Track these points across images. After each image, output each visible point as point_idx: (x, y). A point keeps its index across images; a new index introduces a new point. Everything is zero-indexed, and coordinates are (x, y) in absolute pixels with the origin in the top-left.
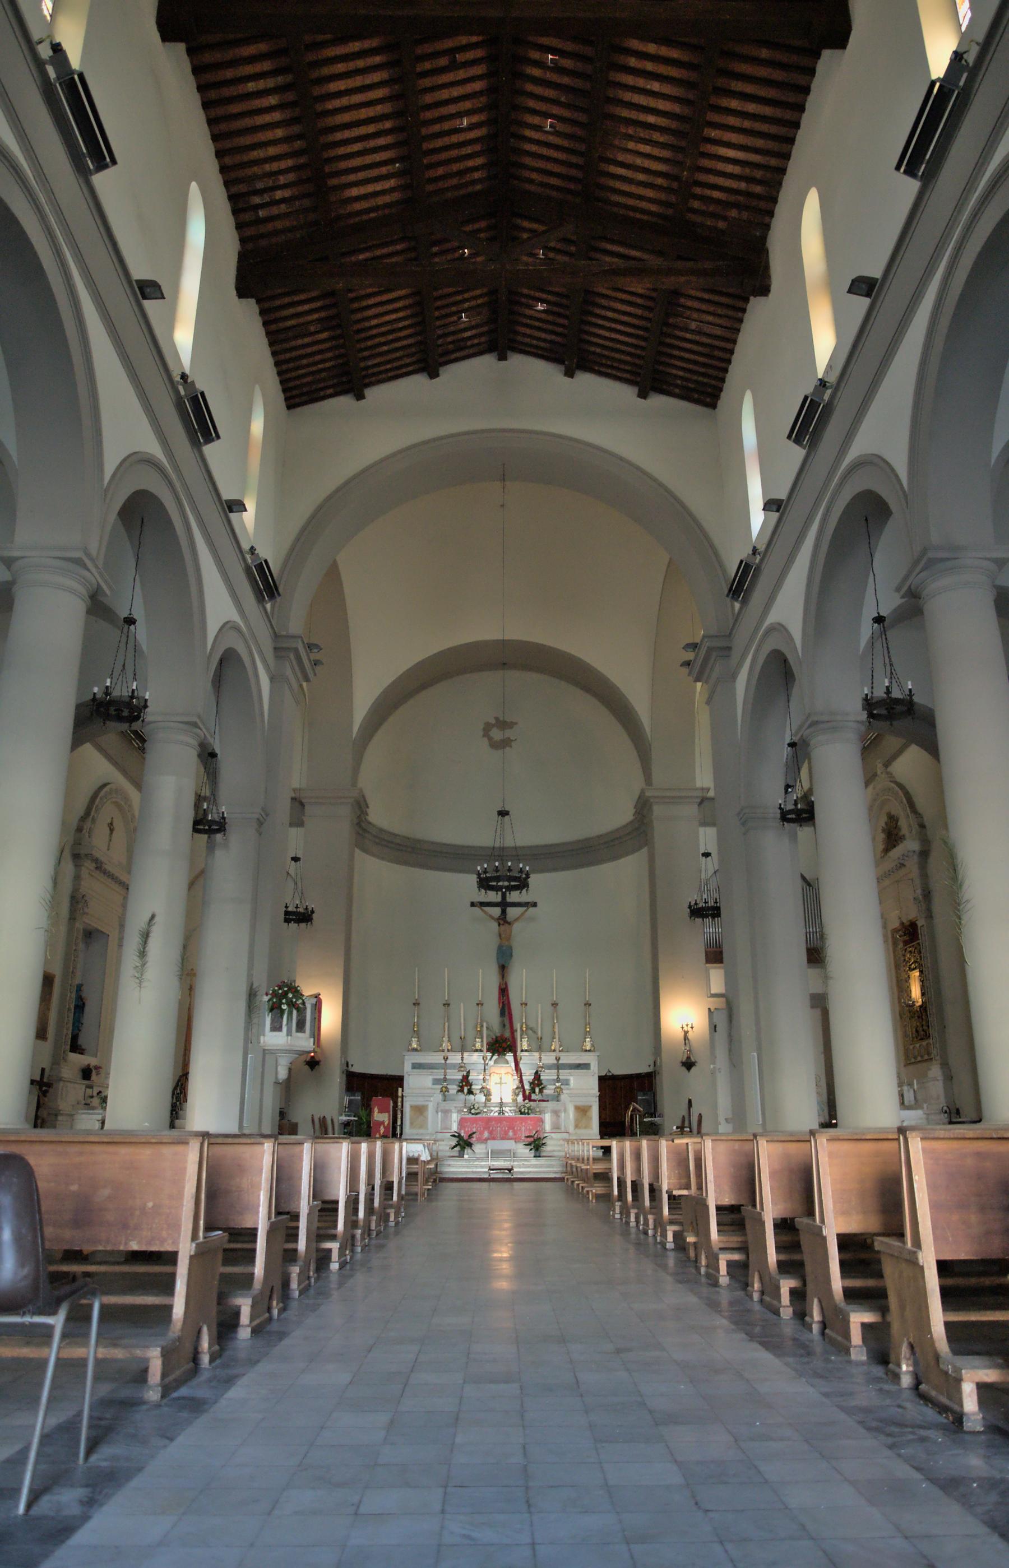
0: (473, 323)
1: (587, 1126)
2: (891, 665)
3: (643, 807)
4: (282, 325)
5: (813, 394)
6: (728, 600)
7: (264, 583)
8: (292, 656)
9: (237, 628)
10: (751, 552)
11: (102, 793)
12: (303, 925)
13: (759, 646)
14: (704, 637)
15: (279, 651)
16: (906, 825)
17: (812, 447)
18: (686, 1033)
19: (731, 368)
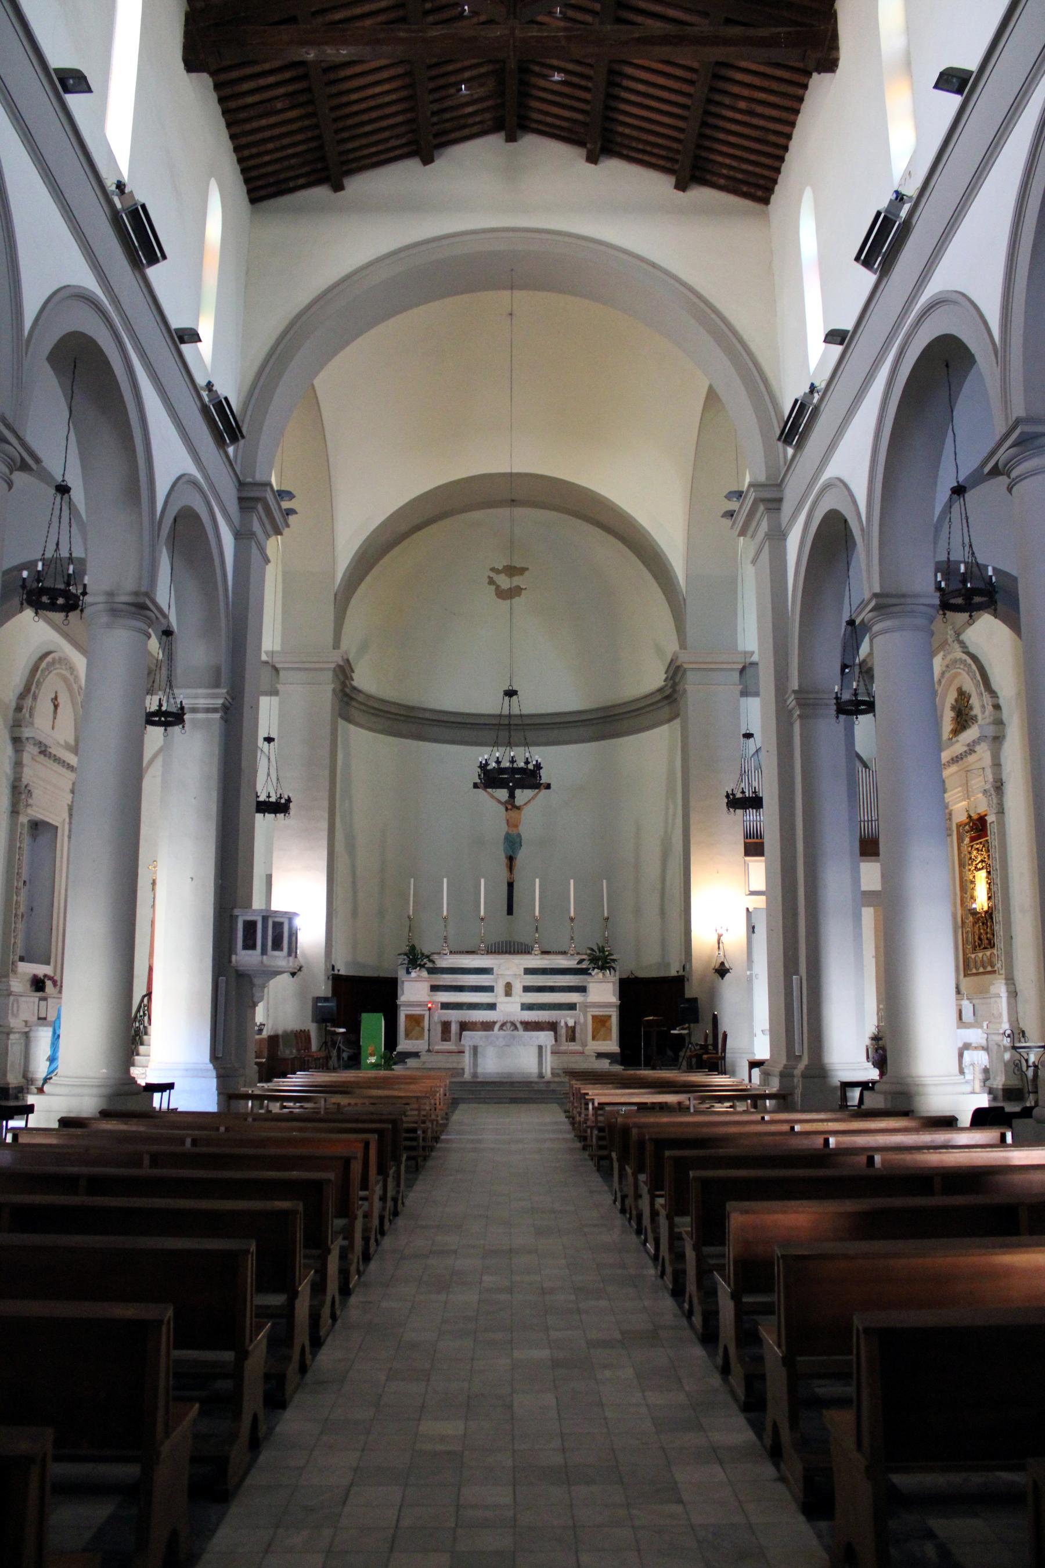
0: (476, 96)
1: (607, 1037)
2: (971, 546)
3: (675, 672)
4: (241, 102)
5: (887, 210)
6: (780, 444)
7: (224, 423)
8: (260, 507)
9: (195, 483)
10: (807, 390)
11: (43, 665)
12: (281, 816)
14: (751, 485)
16: (978, 704)
17: (885, 271)
19: (787, 156)
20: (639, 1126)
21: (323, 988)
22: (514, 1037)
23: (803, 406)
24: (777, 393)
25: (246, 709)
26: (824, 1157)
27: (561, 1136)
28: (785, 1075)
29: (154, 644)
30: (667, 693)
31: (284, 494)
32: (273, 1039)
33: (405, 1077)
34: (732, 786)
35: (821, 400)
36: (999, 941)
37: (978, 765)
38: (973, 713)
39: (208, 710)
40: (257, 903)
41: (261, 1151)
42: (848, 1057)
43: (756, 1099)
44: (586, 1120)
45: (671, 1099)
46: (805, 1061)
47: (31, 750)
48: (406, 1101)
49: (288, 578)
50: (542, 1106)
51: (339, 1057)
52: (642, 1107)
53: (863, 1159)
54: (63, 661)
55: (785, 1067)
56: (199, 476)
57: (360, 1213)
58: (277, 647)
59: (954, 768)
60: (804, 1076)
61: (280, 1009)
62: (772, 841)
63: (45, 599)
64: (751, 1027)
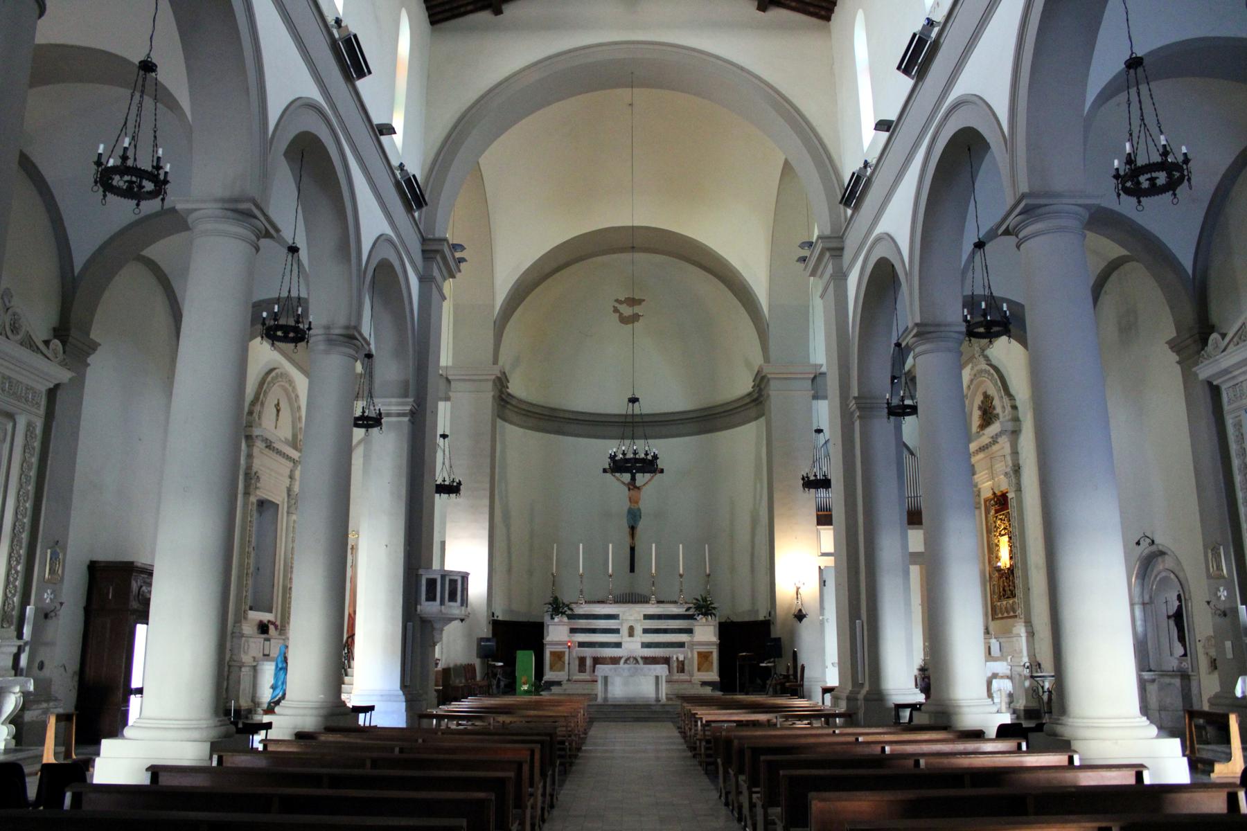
1: (709, 669)
3: (761, 381)
6: (842, 206)
7: (412, 194)
8: (438, 258)
9: (390, 241)
11: (269, 379)
14: (819, 237)
17: (920, 77)
20: (741, 738)
21: (485, 631)
22: (636, 669)
23: (859, 178)
24: (839, 165)
25: (428, 412)
26: (881, 760)
27: (674, 747)
28: (851, 699)
29: (359, 368)
30: (755, 396)
31: (456, 247)
32: (446, 671)
33: (550, 701)
34: (807, 470)
35: (873, 173)
36: (1019, 592)
37: (1000, 453)
39: (399, 415)
40: (436, 565)
41: (452, 757)
42: (900, 684)
43: (828, 717)
44: (696, 734)
45: (762, 717)
46: (866, 688)
47: (259, 445)
48: (555, 719)
49: (456, 307)
50: (659, 724)
51: (498, 686)
52: (740, 724)
53: (911, 762)
54: (285, 376)
55: (851, 692)
57: (529, 804)
58: (450, 364)
59: (981, 455)
60: (866, 699)
61: (453, 647)
62: (838, 513)
63: (279, 333)
64: (824, 661)
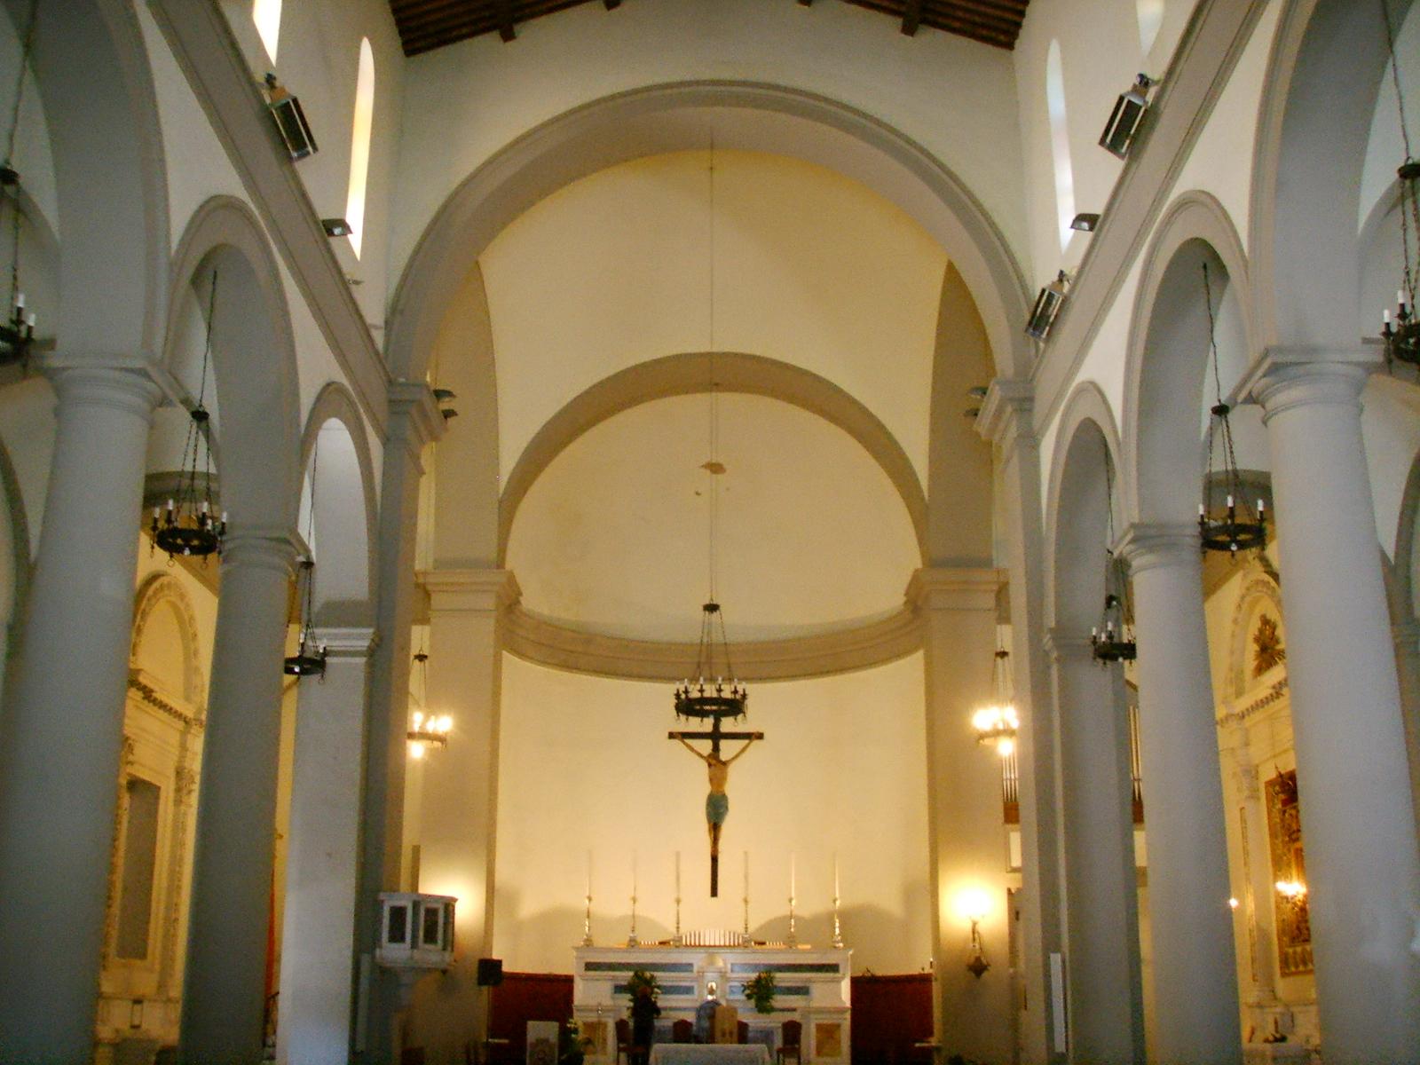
10: (1056, 278)
11: (150, 592)
13: (1069, 408)
15: (394, 404)
17: (1134, 156)
18: (974, 924)
23: (1051, 296)
35: (1072, 290)
38: (1280, 647)
56: (345, 382)
